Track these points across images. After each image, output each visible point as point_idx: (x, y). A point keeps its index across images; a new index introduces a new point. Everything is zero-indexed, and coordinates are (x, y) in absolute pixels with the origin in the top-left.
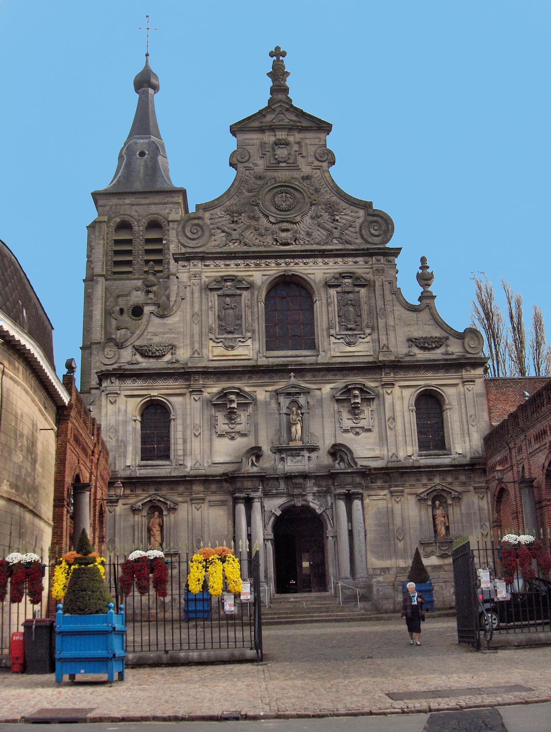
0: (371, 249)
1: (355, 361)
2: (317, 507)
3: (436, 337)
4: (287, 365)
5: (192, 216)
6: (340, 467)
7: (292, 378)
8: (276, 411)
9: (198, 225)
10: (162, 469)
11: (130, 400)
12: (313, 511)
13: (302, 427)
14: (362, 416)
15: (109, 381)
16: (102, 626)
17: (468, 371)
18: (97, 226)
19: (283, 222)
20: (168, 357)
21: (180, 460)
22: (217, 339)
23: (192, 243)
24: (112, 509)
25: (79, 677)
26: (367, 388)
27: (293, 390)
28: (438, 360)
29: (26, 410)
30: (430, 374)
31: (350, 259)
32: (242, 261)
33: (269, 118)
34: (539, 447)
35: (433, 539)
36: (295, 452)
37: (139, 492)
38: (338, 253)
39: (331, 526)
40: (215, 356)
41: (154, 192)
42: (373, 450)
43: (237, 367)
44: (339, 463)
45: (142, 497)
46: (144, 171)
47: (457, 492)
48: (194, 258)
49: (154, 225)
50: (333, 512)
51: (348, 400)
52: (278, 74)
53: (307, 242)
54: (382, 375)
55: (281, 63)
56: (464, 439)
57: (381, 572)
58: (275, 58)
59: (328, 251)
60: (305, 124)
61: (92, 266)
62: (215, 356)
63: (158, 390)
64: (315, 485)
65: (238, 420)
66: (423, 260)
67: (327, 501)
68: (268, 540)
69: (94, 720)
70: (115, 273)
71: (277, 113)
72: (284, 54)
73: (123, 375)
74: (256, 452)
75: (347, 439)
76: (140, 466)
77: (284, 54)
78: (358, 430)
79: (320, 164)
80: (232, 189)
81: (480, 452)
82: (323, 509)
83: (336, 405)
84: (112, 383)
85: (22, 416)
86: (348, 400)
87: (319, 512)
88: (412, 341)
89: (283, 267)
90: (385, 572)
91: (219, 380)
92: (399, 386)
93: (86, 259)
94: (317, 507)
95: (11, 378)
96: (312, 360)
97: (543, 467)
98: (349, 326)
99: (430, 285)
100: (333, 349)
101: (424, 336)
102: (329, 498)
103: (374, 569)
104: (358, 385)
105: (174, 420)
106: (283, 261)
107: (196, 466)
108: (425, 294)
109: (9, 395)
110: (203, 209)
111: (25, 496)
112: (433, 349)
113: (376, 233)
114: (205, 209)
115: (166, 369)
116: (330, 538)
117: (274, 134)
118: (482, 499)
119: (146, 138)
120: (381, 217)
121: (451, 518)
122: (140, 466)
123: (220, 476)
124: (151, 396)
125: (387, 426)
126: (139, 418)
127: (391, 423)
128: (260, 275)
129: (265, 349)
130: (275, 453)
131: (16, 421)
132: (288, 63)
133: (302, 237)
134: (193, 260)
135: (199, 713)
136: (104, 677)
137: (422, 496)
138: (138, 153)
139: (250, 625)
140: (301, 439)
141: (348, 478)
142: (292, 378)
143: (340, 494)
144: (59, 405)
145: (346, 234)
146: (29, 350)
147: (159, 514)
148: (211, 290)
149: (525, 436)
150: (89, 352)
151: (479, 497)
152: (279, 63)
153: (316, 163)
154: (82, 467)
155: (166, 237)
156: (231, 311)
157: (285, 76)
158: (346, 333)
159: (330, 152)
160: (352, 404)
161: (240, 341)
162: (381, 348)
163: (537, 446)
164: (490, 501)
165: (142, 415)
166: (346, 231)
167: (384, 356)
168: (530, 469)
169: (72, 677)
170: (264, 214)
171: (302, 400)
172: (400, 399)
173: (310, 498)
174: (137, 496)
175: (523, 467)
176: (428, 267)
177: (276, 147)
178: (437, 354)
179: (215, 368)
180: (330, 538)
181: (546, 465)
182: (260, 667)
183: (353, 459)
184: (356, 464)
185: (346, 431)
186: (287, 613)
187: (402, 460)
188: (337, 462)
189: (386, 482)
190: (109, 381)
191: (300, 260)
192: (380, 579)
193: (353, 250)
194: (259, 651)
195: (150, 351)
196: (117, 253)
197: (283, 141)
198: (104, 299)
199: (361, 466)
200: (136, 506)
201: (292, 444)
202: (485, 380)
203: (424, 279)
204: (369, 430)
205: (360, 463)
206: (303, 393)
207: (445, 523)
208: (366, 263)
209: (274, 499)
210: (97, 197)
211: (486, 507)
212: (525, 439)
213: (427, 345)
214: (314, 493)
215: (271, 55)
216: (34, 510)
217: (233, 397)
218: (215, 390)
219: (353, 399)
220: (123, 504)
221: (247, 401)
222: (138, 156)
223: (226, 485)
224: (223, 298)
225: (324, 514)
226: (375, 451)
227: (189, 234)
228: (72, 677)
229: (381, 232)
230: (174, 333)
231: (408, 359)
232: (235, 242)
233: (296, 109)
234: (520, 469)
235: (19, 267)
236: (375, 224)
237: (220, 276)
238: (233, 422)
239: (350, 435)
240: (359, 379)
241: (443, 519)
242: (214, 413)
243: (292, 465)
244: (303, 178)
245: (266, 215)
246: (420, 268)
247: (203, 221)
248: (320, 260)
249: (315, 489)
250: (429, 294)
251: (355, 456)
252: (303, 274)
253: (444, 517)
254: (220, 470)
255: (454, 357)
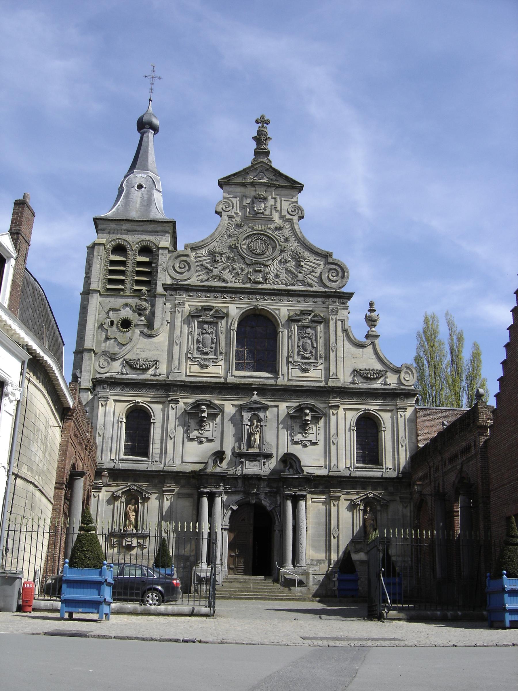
0: (328, 291)
1: (308, 385)
2: (268, 505)
3: (377, 370)
4: (251, 384)
5: (181, 253)
6: (289, 474)
7: (255, 395)
8: (240, 422)
9: (186, 261)
10: (140, 464)
11: (118, 404)
12: (264, 508)
13: (260, 437)
14: (311, 431)
15: (101, 386)
16: (96, 577)
17: (402, 399)
18: (96, 247)
19: (257, 264)
20: (151, 371)
21: (156, 457)
22: (195, 358)
23: (179, 277)
24: (96, 494)
25: (75, 616)
26: (317, 408)
27: (255, 406)
28: (378, 389)
29: (43, 410)
30: (370, 401)
31: (311, 299)
32: (220, 294)
33: (250, 178)
34: (452, 468)
35: (363, 538)
36: (253, 457)
37: (119, 483)
38: (301, 293)
39: (279, 522)
40: (192, 372)
41: (148, 221)
42: (318, 460)
43: (210, 383)
44: (288, 470)
45: (119, 488)
46: (141, 202)
47: (385, 500)
48: (180, 289)
49: (145, 250)
50: (281, 509)
51: (300, 417)
52: (261, 139)
53: (275, 282)
54: (330, 398)
55: (265, 130)
56: (395, 457)
57: (317, 563)
58: (260, 125)
59: (293, 291)
60: (282, 182)
61: (89, 282)
62: (192, 372)
63: (141, 399)
64: (268, 486)
65: (207, 428)
66: (371, 304)
67: (276, 500)
68: (225, 529)
69: (94, 637)
70: (108, 289)
71: (258, 171)
72: (268, 123)
73: (113, 383)
74: (219, 455)
75: (297, 450)
76: (123, 460)
77: (268, 123)
78: (307, 443)
79: (291, 217)
80: (216, 233)
81: (407, 469)
82: (272, 507)
83: (290, 420)
84: (104, 389)
85: (39, 415)
86: (300, 417)
87: (269, 509)
88: (356, 372)
89: (254, 302)
90: (320, 563)
91: (193, 392)
92: (344, 409)
93: (84, 275)
94: (268, 505)
95: (35, 385)
96: (272, 382)
97: (454, 485)
98: (306, 355)
99: (375, 326)
100: (289, 375)
101: (367, 368)
102: (278, 498)
103: (312, 560)
104: (310, 404)
105: (154, 423)
106: (254, 296)
107: (170, 463)
108: (370, 333)
109: (31, 398)
110: (190, 248)
111: (37, 478)
112: (374, 379)
113: (334, 279)
114: (192, 248)
115: (150, 380)
116: (277, 531)
117: (254, 189)
118: (406, 507)
119: (144, 173)
120: (339, 266)
121: (379, 521)
122: (123, 460)
123: (189, 473)
124: (136, 402)
125: (331, 442)
126: (124, 420)
127: (335, 438)
128: (234, 310)
129: (234, 369)
130: (236, 457)
131: (35, 419)
132: (270, 130)
133: (271, 277)
134: (179, 290)
135: (167, 637)
136: (96, 617)
137: (356, 501)
138: (136, 186)
139: (206, 597)
140: (259, 447)
141: (291, 480)
142: (255, 395)
143: (288, 495)
144: (65, 406)
145: (308, 277)
146: (49, 364)
147: (136, 501)
148: (193, 316)
149: (442, 458)
150: (81, 356)
151: (403, 505)
152: (263, 129)
153: (288, 216)
154: (78, 458)
155: (155, 261)
156: (208, 336)
157: (267, 141)
158: (303, 361)
159: (299, 208)
160: (303, 421)
161: (213, 361)
162: (331, 375)
163: (450, 467)
164: (412, 509)
165: (127, 418)
166: (309, 276)
167: (333, 382)
168: (444, 485)
169: (71, 614)
170: (242, 256)
171: (262, 415)
172: (344, 418)
173: (262, 496)
174: (118, 486)
175: (439, 484)
176: (375, 311)
177: (255, 201)
178: (377, 385)
179: (191, 382)
180: (277, 531)
181: (456, 482)
182: (212, 620)
183: (300, 467)
184: (303, 471)
185: (296, 443)
186: (236, 591)
187: (342, 471)
188: (287, 468)
189: (327, 488)
190: (101, 386)
191: (269, 297)
192: (316, 568)
193: (313, 292)
194: (212, 608)
195: (137, 364)
196: (111, 272)
197: (262, 196)
198: (97, 311)
199: (307, 473)
200: (117, 494)
201: (251, 450)
202: (416, 409)
203: (371, 321)
204: (316, 444)
205: (306, 470)
206: (263, 408)
207: (374, 526)
208: (324, 303)
209: (232, 495)
210: (98, 222)
211: (408, 514)
212: (442, 460)
213: (369, 376)
214: (266, 494)
215: (257, 122)
216: (42, 489)
217: (204, 407)
218: (190, 401)
219: (298, 421)
220: (106, 491)
221: (216, 412)
222: (136, 188)
223: (193, 481)
224: (202, 324)
225: (273, 511)
226: (319, 461)
227: (178, 269)
228: (71, 614)
229: (338, 278)
230: (158, 350)
231: (352, 386)
232: (216, 278)
233: (274, 170)
234: (437, 484)
235: (44, 298)
236: (333, 271)
237: (201, 306)
238: (203, 428)
239: (300, 446)
240: (310, 401)
241: (372, 522)
242: (187, 420)
243: (250, 468)
244: (276, 229)
245: (243, 257)
246: (369, 311)
247: (190, 258)
248: (285, 298)
249: (268, 489)
250: (374, 333)
251: (302, 464)
252: (270, 309)
253: (373, 520)
254: (189, 468)
255: (391, 387)
